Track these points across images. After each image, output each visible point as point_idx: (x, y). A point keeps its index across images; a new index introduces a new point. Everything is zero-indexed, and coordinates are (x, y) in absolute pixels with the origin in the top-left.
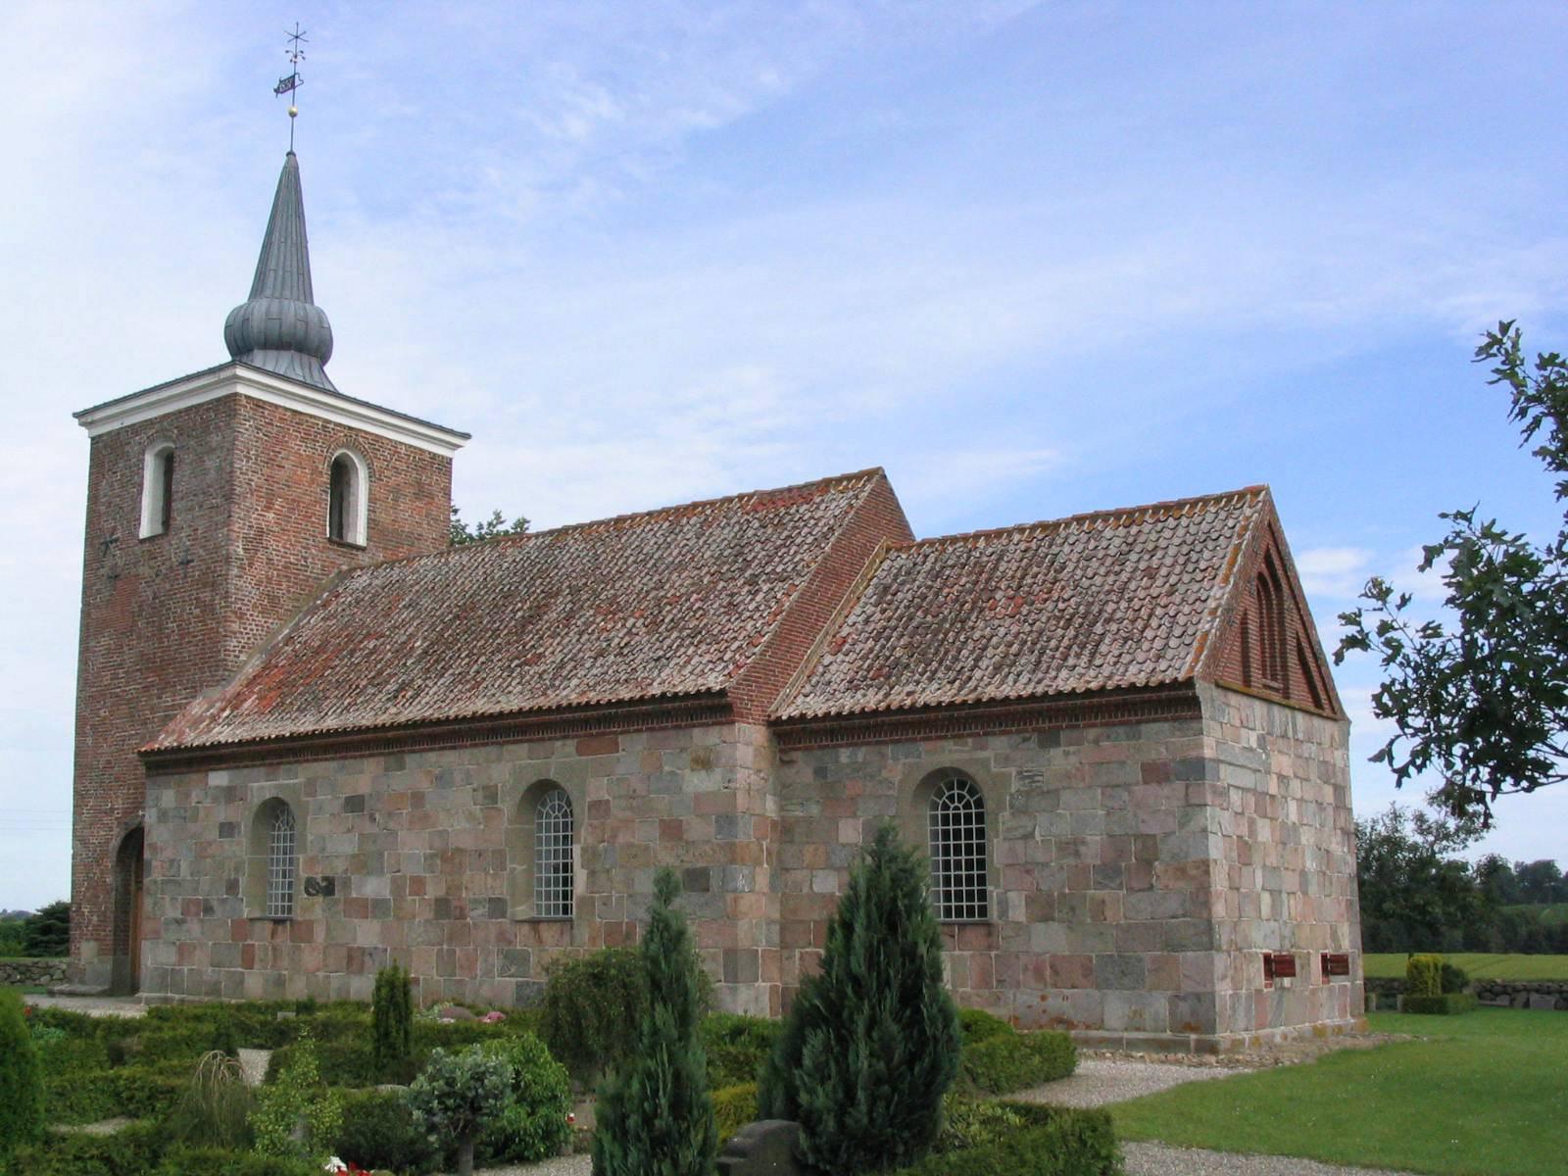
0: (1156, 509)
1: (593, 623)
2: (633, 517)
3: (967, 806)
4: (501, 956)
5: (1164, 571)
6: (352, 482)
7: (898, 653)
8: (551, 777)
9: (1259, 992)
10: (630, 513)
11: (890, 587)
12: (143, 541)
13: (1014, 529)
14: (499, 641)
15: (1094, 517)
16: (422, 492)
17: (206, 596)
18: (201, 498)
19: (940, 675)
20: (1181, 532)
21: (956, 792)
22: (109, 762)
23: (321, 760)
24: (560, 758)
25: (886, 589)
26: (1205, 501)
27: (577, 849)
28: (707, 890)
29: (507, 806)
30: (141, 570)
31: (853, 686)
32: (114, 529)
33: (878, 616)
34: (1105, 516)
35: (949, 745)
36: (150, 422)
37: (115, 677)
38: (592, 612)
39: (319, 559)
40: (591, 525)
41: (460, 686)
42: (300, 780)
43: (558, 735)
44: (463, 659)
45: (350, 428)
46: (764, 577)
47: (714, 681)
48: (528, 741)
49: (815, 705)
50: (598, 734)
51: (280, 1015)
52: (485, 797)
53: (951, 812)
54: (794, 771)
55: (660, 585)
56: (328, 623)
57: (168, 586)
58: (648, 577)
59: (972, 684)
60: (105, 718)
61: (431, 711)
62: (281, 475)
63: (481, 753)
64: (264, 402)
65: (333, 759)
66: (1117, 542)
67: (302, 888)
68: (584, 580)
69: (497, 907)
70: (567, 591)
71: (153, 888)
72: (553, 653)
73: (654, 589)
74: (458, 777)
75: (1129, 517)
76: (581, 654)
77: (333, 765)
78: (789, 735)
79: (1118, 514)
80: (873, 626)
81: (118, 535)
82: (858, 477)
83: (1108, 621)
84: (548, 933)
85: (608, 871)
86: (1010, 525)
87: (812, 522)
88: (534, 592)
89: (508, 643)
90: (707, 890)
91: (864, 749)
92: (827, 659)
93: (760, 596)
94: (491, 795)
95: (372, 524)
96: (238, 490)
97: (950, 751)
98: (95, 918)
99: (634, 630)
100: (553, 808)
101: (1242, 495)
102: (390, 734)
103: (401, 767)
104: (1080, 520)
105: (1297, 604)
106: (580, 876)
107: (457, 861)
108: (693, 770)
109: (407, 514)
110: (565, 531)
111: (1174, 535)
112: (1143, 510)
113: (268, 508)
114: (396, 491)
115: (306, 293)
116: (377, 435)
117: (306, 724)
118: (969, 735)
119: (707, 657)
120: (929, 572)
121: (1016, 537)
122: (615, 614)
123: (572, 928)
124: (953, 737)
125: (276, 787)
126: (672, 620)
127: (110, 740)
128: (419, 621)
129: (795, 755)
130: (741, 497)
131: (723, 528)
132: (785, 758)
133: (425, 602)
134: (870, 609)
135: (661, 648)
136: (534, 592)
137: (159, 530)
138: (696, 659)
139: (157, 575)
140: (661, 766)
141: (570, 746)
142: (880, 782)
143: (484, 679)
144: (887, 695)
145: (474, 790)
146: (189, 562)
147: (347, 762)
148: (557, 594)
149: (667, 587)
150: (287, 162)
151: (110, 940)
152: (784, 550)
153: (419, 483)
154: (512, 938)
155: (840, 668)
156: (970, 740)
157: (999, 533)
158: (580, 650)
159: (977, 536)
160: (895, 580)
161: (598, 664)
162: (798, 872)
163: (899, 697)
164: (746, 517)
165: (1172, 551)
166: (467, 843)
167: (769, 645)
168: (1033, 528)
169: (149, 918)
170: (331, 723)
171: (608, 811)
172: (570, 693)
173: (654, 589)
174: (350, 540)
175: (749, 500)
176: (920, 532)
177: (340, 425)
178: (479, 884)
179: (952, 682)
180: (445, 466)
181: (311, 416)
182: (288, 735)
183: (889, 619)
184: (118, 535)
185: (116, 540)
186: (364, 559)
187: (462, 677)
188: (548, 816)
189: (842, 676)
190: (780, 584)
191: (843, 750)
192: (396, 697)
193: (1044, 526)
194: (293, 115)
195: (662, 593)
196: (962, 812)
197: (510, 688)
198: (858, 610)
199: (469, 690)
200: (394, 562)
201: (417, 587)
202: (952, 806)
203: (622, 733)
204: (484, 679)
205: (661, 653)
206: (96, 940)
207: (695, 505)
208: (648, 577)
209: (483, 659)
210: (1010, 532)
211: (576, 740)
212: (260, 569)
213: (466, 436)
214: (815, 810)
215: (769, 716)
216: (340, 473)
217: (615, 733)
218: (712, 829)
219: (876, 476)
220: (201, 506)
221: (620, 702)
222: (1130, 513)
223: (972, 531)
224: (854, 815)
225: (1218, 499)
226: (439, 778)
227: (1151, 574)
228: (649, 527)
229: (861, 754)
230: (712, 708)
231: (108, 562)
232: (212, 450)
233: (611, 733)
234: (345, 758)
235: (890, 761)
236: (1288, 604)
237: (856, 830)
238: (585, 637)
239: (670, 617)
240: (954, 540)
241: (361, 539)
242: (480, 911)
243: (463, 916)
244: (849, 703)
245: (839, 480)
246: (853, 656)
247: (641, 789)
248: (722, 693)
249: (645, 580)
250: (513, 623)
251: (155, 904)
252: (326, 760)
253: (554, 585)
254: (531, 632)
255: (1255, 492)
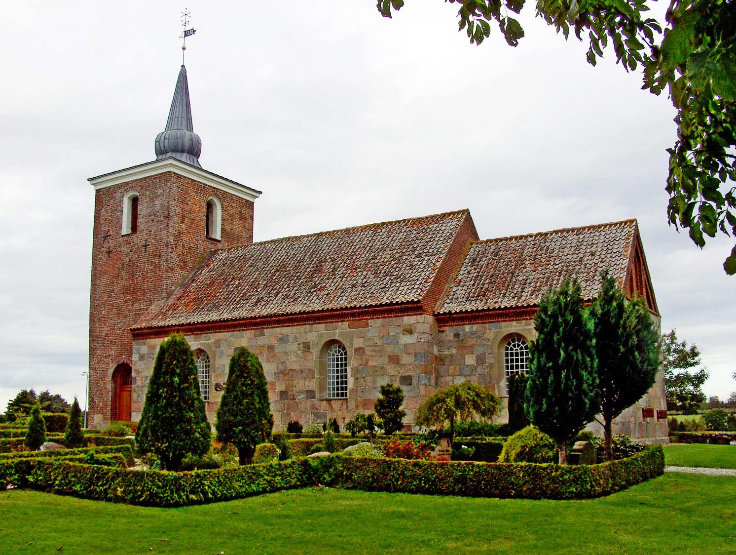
0: (589, 228)
1: (346, 273)
2: (354, 228)
3: (521, 349)
4: (313, 415)
5: (598, 253)
6: (214, 212)
7: (486, 286)
8: (336, 338)
9: (640, 423)
10: (597, 224)
11: (476, 259)
12: (123, 236)
13: (528, 236)
14: (301, 281)
15: (562, 231)
16: (242, 217)
17: (156, 260)
18: (153, 217)
19: (507, 295)
20: (602, 237)
21: (516, 343)
22: (107, 334)
23: (223, 332)
24: (340, 330)
25: (474, 260)
26: (610, 225)
27: (349, 369)
28: (411, 384)
29: (315, 351)
30: (122, 249)
31: (468, 299)
32: (109, 230)
33: (473, 271)
34: (568, 231)
35: (514, 323)
36: (127, 183)
37: (110, 296)
38: (344, 269)
39: (202, 245)
40: (333, 232)
41: (288, 300)
42: (212, 341)
43: (339, 320)
44: (285, 289)
45: (214, 188)
46: (424, 254)
47: (413, 297)
48: (324, 323)
49: (454, 308)
50: (359, 320)
51: (136, 448)
52: (304, 347)
53: (514, 351)
54: (445, 335)
55: (375, 258)
56: (211, 273)
57: (136, 257)
58: (368, 254)
59: (523, 298)
60: (105, 315)
61: (276, 311)
62: (188, 208)
63: (302, 328)
64: (182, 176)
65: (228, 331)
66: (575, 241)
67: (214, 388)
68: (337, 255)
69: (310, 394)
70: (329, 260)
71: (137, 389)
72: (330, 286)
73: (373, 259)
74: (291, 339)
75: (579, 231)
76: (344, 286)
77: (229, 334)
78: (443, 320)
79: (573, 230)
80: (472, 275)
81: (111, 233)
82: (458, 212)
83: (577, 273)
84: (336, 405)
85: (364, 378)
86: (526, 234)
87: (441, 232)
88: (313, 260)
89: (306, 282)
90: (411, 384)
91: (476, 325)
92: (454, 289)
93: (424, 262)
94: (307, 347)
95: (223, 230)
96: (171, 214)
97: (515, 326)
98: (101, 404)
99: (367, 276)
100: (335, 351)
101: (626, 223)
102: (258, 320)
103: (263, 335)
104: (556, 232)
105: (645, 267)
106: (351, 381)
107: (291, 375)
108: (404, 334)
109: (237, 227)
110: (320, 235)
111: (600, 238)
112: (584, 228)
113: (182, 222)
114: (232, 215)
115: (190, 127)
116: (225, 191)
117: (214, 316)
118: (523, 319)
119: (407, 287)
120: (492, 253)
121: (530, 239)
122: (356, 269)
123: (347, 402)
124: (516, 320)
125: (200, 344)
126: (385, 272)
127: (107, 324)
128: (258, 273)
129: (444, 328)
130: (404, 220)
131: (399, 234)
132: (441, 330)
133: (260, 264)
134: (469, 268)
135: (383, 284)
136: (313, 260)
137: (130, 231)
138: (401, 288)
139: (131, 251)
140: (389, 333)
141: (345, 324)
142: (483, 339)
143: (299, 297)
144: (486, 303)
145: (299, 344)
146: (147, 245)
147: (235, 333)
148: (325, 262)
149: (378, 258)
150: (182, 69)
151: (109, 414)
152: (431, 243)
153: (241, 213)
154: (319, 407)
155: (461, 292)
156: (524, 321)
157: (521, 237)
158: (343, 285)
159: (511, 239)
160: (478, 256)
161: (354, 290)
162: (447, 377)
163: (491, 304)
164: (408, 229)
165: (600, 245)
166: (296, 366)
167: (433, 282)
168: (537, 235)
169: (135, 402)
170: (226, 316)
171: (364, 352)
172: (343, 303)
173: (373, 259)
174: (213, 237)
175: (408, 222)
176: (483, 237)
177: (211, 187)
178: (301, 384)
179: (514, 298)
180: (251, 205)
181: (199, 182)
182: (448, 312)
183: (478, 272)
184: (111, 233)
185: (109, 236)
186: (220, 246)
187: (286, 297)
188: (333, 355)
189: (463, 296)
190: (433, 257)
191: (467, 326)
192: (257, 305)
193: (541, 234)
194: (184, 49)
195: (377, 261)
196: (519, 351)
197: (313, 301)
198: (463, 269)
199: (292, 302)
200: (238, 247)
201: (253, 258)
202: (514, 349)
203: (370, 319)
204: (299, 297)
205: (384, 286)
206: (101, 413)
207: (383, 224)
208: (368, 254)
209: (296, 288)
210: (526, 237)
211: (348, 322)
212: (180, 249)
213: (260, 193)
214: (454, 351)
215: (434, 312)
216: (210, 206)
217: (367, 319)
218: (413, 359)
219: (467, 212)
220: (153, 221)
221: (371, 306)
222: (579, 229)
223: (509, 236)
224: (472, 353)
225: (616, 224)
226: (281, 339)
227: (593, 254)
228: (362, 233)
229: (475, 327)
230: (414, 308)
231: (106, 245)
232: (157, 197)
233: (364, 319)
234: (234, 331)
235: (488, 330)
236: (642, 267)
237: (473, 359)
238: (344, 279)
239: (384, 271)
240: (501, 240)
241: (219, 238)
242: (302, 396)
243: (294, 399)
244: (469, 307)
245: (450, 214)
246: (465, 288)
247: (379, 343)
248: (419, 301)
249: (367, 256)
250: (306, 273)
251: (138, 396)
252: (225, 332)
253: (322, 257)
254: (316, 277)
255: (632, 221)
